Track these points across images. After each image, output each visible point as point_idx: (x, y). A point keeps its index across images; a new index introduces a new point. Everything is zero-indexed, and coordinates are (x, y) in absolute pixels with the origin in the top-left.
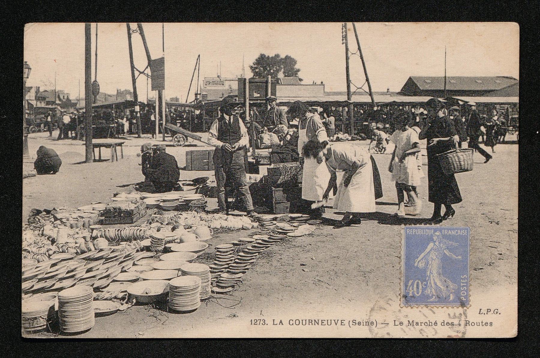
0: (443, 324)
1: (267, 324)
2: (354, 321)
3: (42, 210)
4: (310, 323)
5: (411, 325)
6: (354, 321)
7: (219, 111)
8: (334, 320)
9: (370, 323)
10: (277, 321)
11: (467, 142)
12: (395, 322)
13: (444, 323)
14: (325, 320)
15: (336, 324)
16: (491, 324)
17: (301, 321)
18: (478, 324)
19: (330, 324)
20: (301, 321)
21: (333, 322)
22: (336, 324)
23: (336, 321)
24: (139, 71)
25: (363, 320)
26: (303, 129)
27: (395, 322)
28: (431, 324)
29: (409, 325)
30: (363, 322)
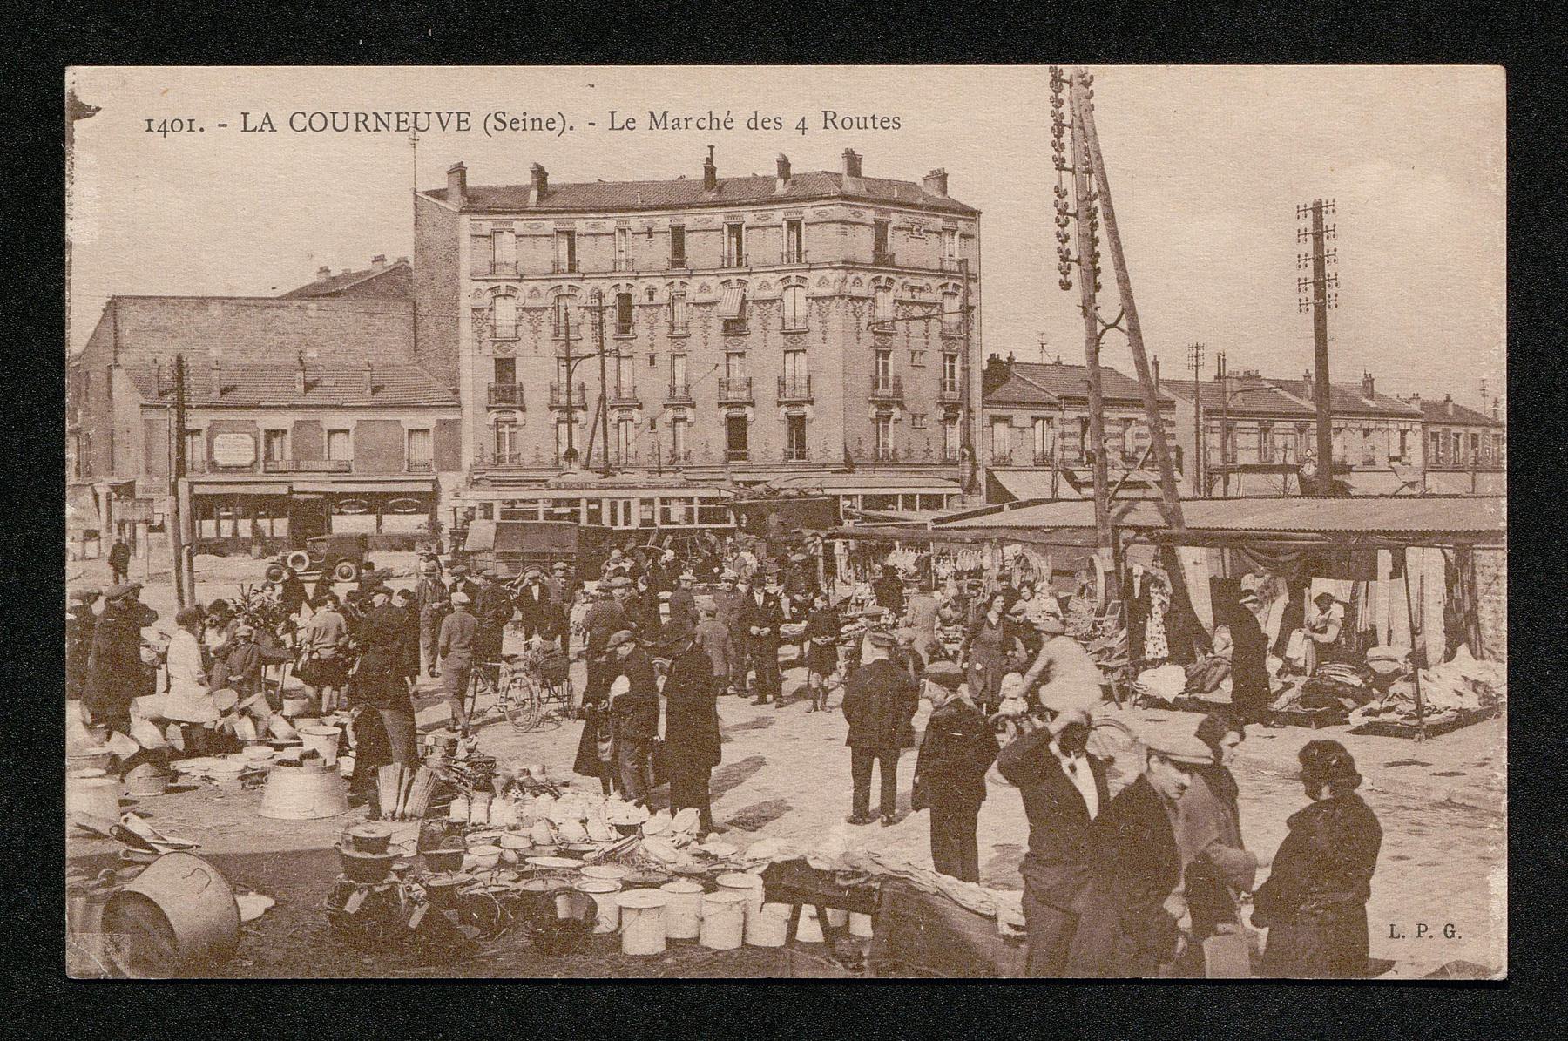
0: (752, 124)
1: (571, 128)
2: (778, 120)
3: (1289, 654)
4: (361, 126)
5: (658, 126)
6: (778, 120)
7: (919, 739)
8: (439, 113)
9: (721, 123)
10: (255, 120)
11: (1179, 894)
12: (245, 117)
13: (756, 119)
14: (407, 113)
15: (444, 128)
16: (896, 120)
17: (855, 121)
18: (537, 123)
19: (503, 126)
20: (855, 121)
21: (434, 117)
22: (444, 128)
23: (444, 117)
24: (1119, 328)
25: (525, 114)
26: (1174, 407)
27: (245, 117)
28: (715, 122)
29: (381, 126)
30: (524, 120)
